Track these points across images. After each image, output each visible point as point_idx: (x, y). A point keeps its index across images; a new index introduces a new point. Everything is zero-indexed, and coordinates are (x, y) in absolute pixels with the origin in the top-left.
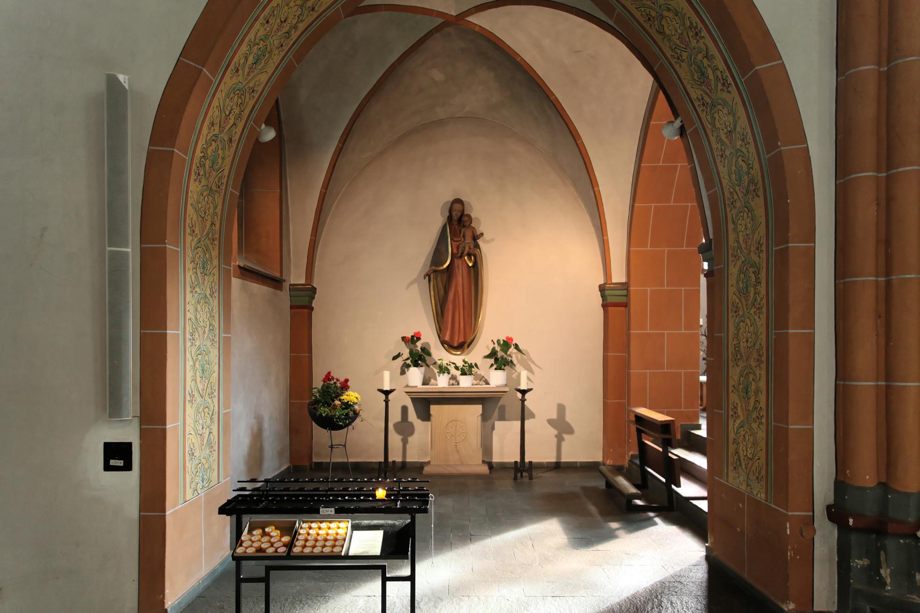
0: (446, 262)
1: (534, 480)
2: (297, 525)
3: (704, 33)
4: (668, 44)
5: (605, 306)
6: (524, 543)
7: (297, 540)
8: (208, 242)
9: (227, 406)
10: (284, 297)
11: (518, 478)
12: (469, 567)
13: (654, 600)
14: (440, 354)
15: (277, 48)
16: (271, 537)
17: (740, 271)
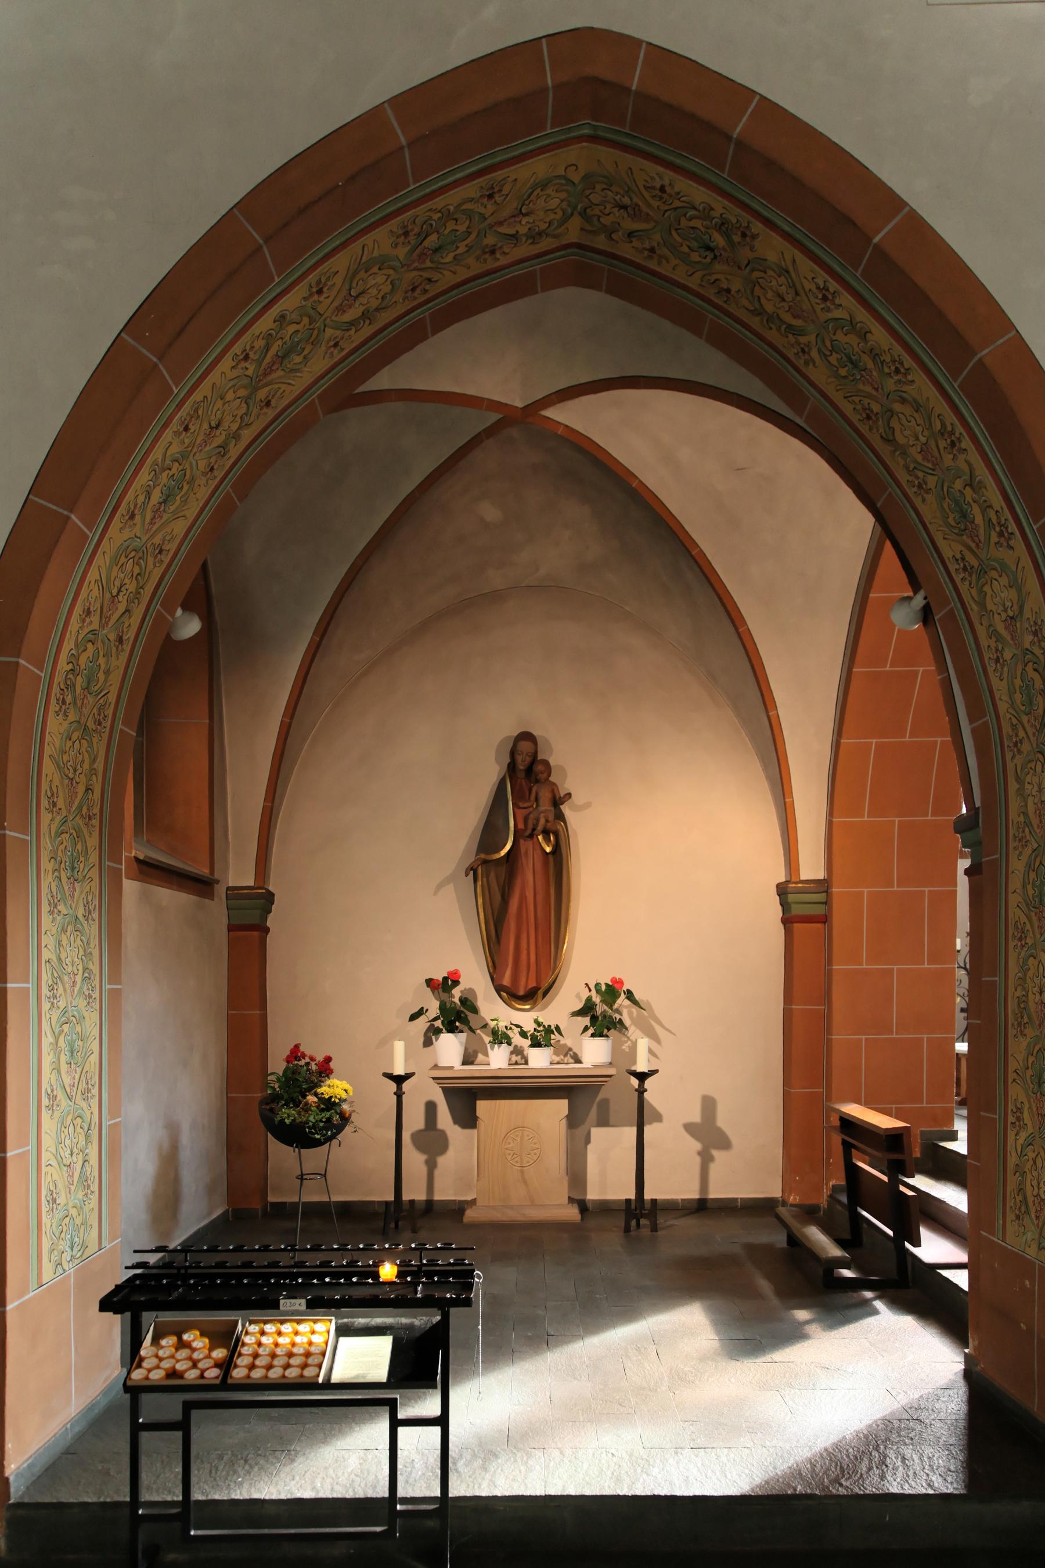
0: (505, 845)
1: (659, 1233)
2: (240, 1327)
3: (966, 443)
4: (902, 462)
5: (787, 921)
6: (643, 1350)
7: (240, 1355)
8: (80, 822)
9: (115, 1113)
10: (217, 910)
11: (632, 1229)
12: (545, 1394)
13: (873, 1454)
15: (205, 474)
16: (194, 1350)
17: (1029, 867)
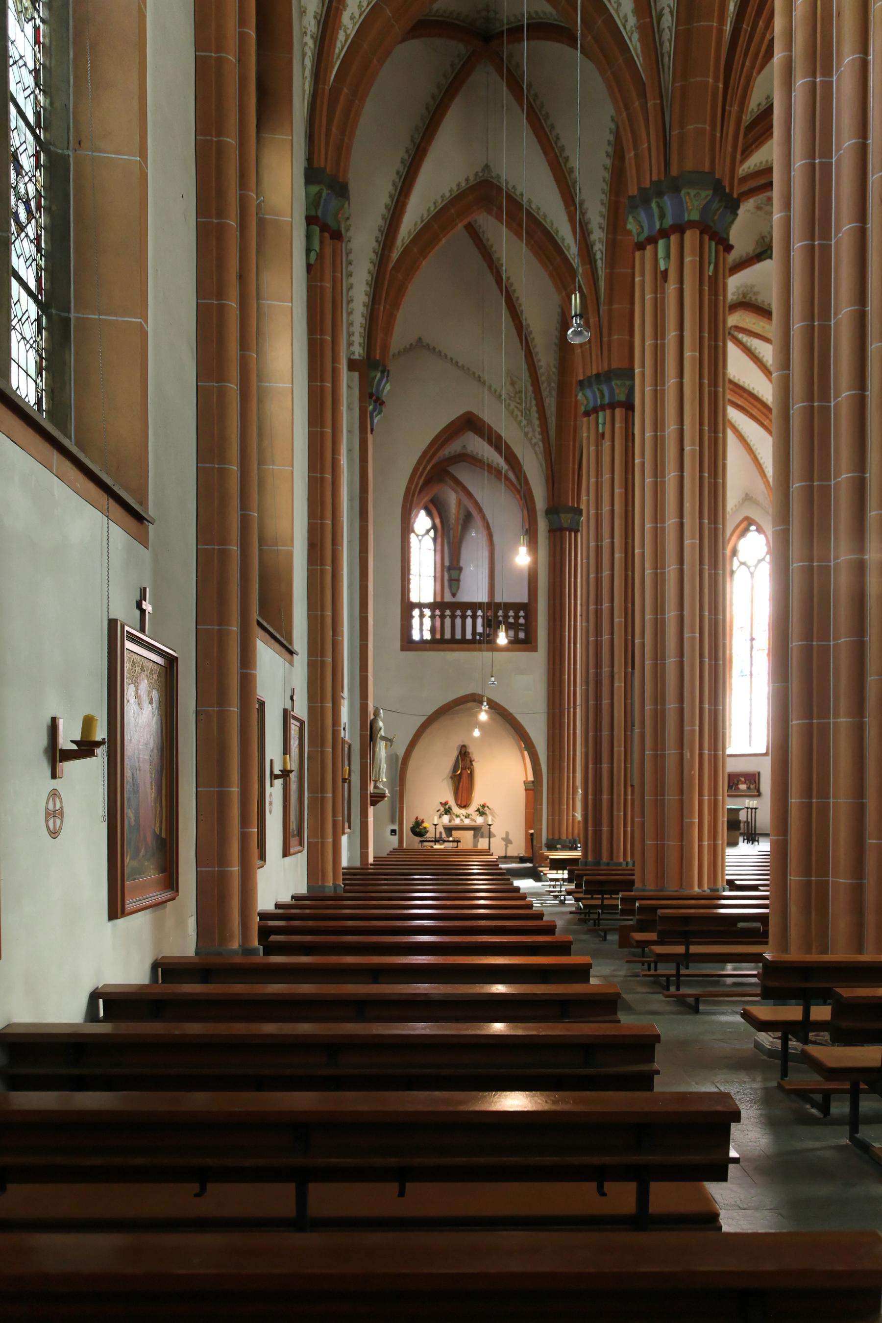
14: (456, 810)
